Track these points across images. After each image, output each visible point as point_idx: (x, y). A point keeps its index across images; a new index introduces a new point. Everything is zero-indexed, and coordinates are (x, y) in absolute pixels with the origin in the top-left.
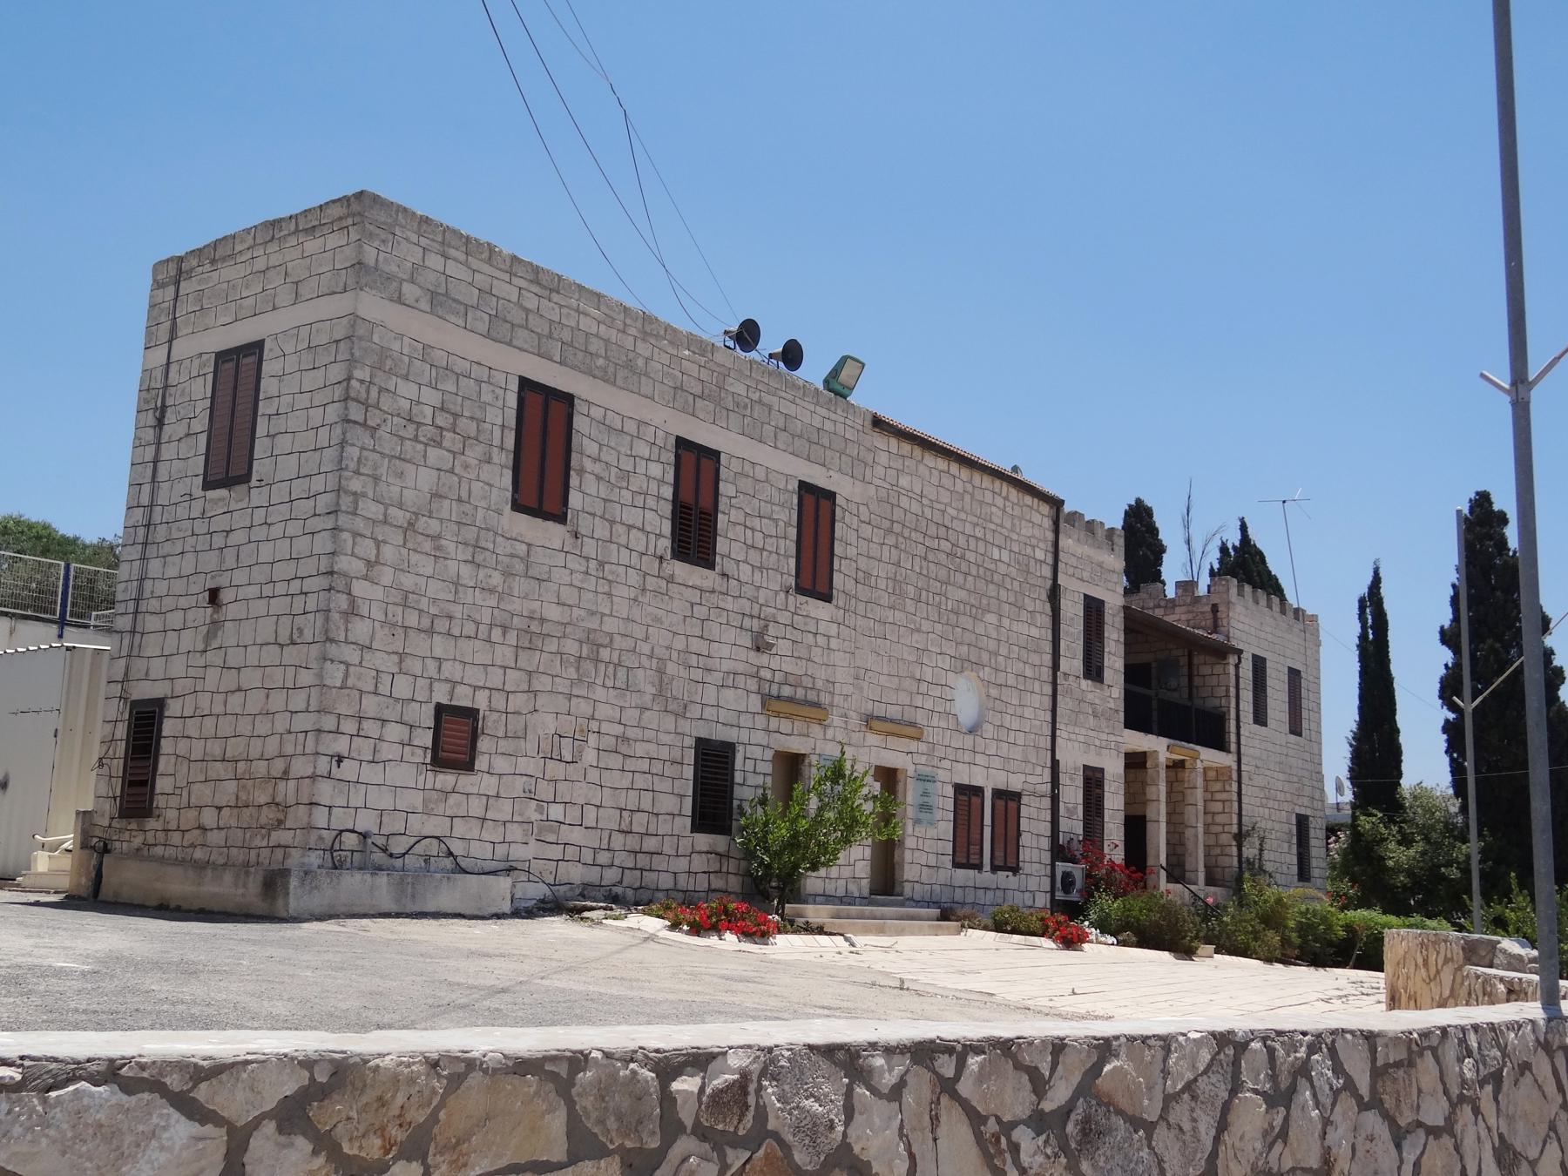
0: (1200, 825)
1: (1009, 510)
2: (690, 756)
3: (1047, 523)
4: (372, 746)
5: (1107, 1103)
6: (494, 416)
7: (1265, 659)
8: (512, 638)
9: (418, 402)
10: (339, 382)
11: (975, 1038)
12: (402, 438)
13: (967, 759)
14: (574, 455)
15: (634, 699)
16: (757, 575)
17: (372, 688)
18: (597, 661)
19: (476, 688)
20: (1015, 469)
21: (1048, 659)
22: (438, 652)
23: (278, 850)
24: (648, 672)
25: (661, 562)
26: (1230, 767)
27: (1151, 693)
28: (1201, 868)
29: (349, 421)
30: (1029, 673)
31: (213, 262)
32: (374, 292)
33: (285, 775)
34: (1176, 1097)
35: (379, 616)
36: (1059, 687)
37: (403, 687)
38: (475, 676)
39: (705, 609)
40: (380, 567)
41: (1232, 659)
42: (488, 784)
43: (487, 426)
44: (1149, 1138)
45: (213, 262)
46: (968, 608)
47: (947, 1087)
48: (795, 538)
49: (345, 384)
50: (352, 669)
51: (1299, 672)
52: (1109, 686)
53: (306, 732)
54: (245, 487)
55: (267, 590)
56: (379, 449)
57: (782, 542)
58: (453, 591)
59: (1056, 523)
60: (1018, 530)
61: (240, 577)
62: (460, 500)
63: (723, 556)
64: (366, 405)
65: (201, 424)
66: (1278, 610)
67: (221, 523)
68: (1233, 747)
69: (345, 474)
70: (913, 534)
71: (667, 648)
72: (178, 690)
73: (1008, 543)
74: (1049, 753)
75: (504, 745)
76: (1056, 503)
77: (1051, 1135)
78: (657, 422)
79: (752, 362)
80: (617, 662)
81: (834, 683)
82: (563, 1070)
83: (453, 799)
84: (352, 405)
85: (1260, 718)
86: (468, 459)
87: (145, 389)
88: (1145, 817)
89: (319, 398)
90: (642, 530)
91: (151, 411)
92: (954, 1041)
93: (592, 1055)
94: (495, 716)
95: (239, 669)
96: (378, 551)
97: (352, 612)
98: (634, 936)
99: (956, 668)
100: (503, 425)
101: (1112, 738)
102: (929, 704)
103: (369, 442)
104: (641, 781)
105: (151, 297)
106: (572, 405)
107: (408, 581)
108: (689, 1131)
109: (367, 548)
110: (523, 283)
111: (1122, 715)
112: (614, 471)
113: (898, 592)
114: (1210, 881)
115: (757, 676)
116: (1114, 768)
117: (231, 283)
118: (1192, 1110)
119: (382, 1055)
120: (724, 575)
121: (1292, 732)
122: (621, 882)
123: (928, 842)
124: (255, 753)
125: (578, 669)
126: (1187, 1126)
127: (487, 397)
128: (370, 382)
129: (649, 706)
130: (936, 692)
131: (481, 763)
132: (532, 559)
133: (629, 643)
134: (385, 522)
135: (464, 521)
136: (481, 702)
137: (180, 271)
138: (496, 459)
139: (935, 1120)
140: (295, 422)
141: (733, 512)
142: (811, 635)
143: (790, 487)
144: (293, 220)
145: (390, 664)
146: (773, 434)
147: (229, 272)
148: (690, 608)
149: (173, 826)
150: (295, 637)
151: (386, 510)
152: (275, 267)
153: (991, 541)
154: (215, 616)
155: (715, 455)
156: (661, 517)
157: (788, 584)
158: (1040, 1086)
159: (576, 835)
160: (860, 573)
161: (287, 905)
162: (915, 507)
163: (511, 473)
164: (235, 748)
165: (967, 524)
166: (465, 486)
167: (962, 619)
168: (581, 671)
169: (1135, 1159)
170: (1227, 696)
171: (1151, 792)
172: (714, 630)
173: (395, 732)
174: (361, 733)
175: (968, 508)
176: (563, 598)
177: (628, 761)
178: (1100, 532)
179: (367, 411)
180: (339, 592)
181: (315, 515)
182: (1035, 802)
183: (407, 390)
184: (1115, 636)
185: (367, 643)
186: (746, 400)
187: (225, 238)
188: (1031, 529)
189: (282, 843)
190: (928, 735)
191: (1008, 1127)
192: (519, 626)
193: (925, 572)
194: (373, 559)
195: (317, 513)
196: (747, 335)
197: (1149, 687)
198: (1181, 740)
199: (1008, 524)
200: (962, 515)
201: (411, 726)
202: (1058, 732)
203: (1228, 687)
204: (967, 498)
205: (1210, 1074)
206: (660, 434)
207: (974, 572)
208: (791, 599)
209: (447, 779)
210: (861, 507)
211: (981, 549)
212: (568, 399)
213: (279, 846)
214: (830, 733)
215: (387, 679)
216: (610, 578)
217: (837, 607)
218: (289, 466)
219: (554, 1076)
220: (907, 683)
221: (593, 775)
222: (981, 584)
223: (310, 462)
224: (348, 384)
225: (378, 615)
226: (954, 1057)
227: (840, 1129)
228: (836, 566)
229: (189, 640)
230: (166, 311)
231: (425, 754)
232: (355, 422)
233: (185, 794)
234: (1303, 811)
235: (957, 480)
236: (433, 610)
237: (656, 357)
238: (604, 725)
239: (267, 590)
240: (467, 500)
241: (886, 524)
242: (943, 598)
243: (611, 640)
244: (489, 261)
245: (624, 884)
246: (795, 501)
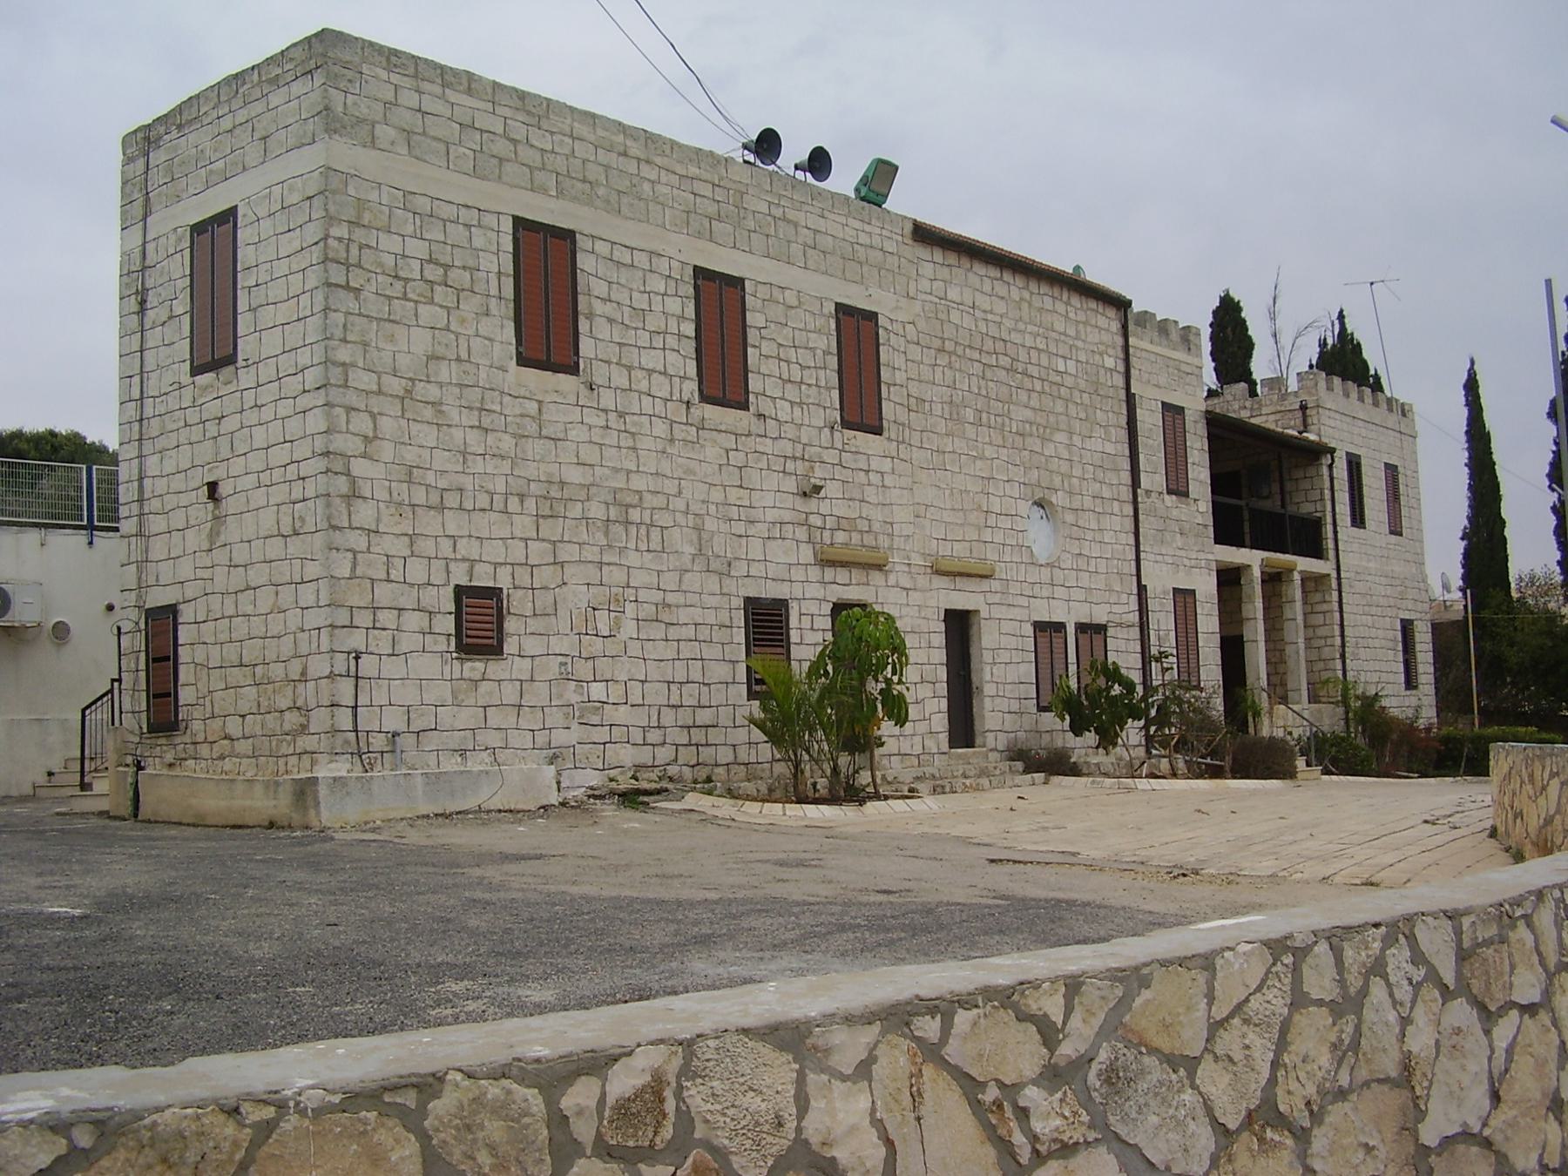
0: (1301, 640)
1: (1072, 315)
2: (739, 619)
3: (1115, 326)
4: (390, 638)
5: (1142, 1045)
6: (489, 263)
7: (1360, 456)
8: (531, 504)
9: (404, 256)
10: (316, 243)
11: (964, 992)
12: (389, 298)
13: (1045, 593)
14: (581, 298)
15: (673, 562)
16: (797, 411)
17: (384, 576)
18: (628, 523)
19: (496, 565)
20: (1077, 268)
21: (1126, 477)
22: (452, 530)
23: (305, 756)
24: (685, 529)
25: (688, 408)
26: (1329, 575)
27: (1242, 503)
28: (1304, 686)
29: (329, 285)
30: (1106, 493)
31: (180, 127)
32: (344, 139)
33: (304, 678)
34: (1222, 1023)
35: (385, 496)
36: (1140, 505)
37: (417, 571)
38: (495, 552)
39: (742, 455)
40: (378, 442)
41: (1326, 460)
42: (521, 668)
43: (483, 275)
44: (1192, 1075)
45: (180, 127)
46: (1034, 428)
47: (932, 1052)
48: (836, 367)
49: (322, 244)
50: (359, 556)
51: (1396, 467)
52: (1195, 500)
53: (319, 629)
54: (231, 368)
55: (265, 478)
56: (365, 313)
57: (821, 373)
58: (461, 460)
59: (1125, 327)
60: (1083, 337)
61: (238, 466)
62: (458, 360)
63: (757, 394)
64: (348, 266)
65: (182, 306)
66: (1371, 402)
67: (213, 409)
68: (1331, 554)
69: (332, 343)
70: (967, 350)
71: (703, 502)
72: (189, 594)
73: (1074, 351)
74: (1135, 578)
75: (534, 625)
76: (1120, 304)
77: (1069, 1092)
78: (672, 252)
79: (771, 174)
80: (649, 522)
81: (892, 524)
82: (409, 1099)
83: (484, 687)
84: (332, 267)
85: (1358, 519)
86: (462, 313)
87: (125, 274)
88: (1242, 636)
89: (298, 263)
90: (665, 373)
91: (133, 296)
92: (937, 999)
93: (449, 1077)
94: (520, 593)
95: (245, 566)
96: (375, 426)
97: (353, 495)
98: (689, 819)
99: (1025, 495)
100: (499, 272)
101: (1202, 556)
102: (999, 538)
103: (353, 306)
104: (687, 650)
105: (123, 173)
106: (574, 242)
107: (410, 455)
108: (589, 1152)
109: (362, 423)
110: (508, 112)
111: (1211, 529)
112: (627, 310)
113: (955, 417)
114: (1314, 698)
115: (806, 523)
116: (1206, 587)
117: (199, 148)
118: (1244, 1036)
119: (159, 1109)
120: (761, 416)
121: (1392, 532)
122: (676, 760)
123: (1008, 687)
124: (271, 655)
125: (606, 534)
126: (1238, 1055)
127: (478, 242)
128: (349, 239)
129: (690, 567)
130: (1005, 523)
131: (510, 647)
132: (545, 417)
133: (659, 501)
134: (380, 392)
135: (466, 382)
136: (504, 582)
137: (147, 139)
138: (494, 309)
139: (916, 1097)
140: (277, 291)
141: (764, 344)
142: (862, 474)
143: (826, 311)
144: (256, 72)
145: (400, 547)
146: (801, 253)
147: (198, 138)
148: (725, 456)
149: (200, 738)
150: (297, 526)
151: (379, 378)
152: (241, 124)
153: (1055, 351)
154: (217, 512)
155: (737, 283)
156: (685, 357)
157: (832, 419)
158: (1049, 1034)
159: (622, 714)
160: (911, 399)
161: (318, 813)
162: (968, 322)
163: (513, 324)
164: (250, 652)
165: (1027, 336)
166: (463, 342)
167: (1029, 440)
168: (610, 536)
169: (1175, 1103)
170: (1322, 499)
171: (1247, 610)
172: (753, 477)
173: (414, 621)
174: (377, 625)
175: (1026, 318)
176: (583, 457)
177: (672, 629)
178: (1174, 331)
179: (348, 271)
180: (336, 473)
181: (304, 391)
182: (1122, 633)
183: (390, 243)
184: (1198, 445)
185: (373, 527)
186: (769, 218)
187: (191, 98)
188: (1097, 335)
189: (308, 749)
190: (1001, 571)
191: (1011, 1089)
192: (539, 493)
193: (984, 393)
194: (371, 434)
195: (306, 388)
196: (767, 144)
197: (1240, 499)
198: (1275, 551)
199: (1072, 332)
200: (1021, 326)
201: (430, 613)
202: (1143, 555)
203: (1322, 490)
204: (1025, 306)
205: (1265, 990)
206: (675, 264)
207: (1038, 388)
208: (837, 435)
209: (475, 667)
210: (907, 326)
211: (1045, 362)
212: (567, 237)
213: (306, 752)
214: (892, 579)
215: (399, 563)
216: (633, 430)
217: (889, 439)
218: (272, 342)
219: (402, 1112)
220: (973, 517)
221: (634, 649)
222: (1047, 401)
223: (294, 335)
224: (325, 244)
225: (382, 495)
226: (938, 1017)
227: (791, 1125)
228: (884, 394)
229: (195, 539)
230: (138, 188)
231: (448, 640)
232: (337, 286)
233: (208, 704)
234: (1407, 616)
235: (1012, 287)
236: (442, 484)
237: (664, 179)
238: (641, 592)
239: (265, 478)
240: (466, 358)
241: (937, 343)
242: (1007, 420)
243: (641, 499)
244: (469, 91)
245: (680, 762)
246: (833, 326)
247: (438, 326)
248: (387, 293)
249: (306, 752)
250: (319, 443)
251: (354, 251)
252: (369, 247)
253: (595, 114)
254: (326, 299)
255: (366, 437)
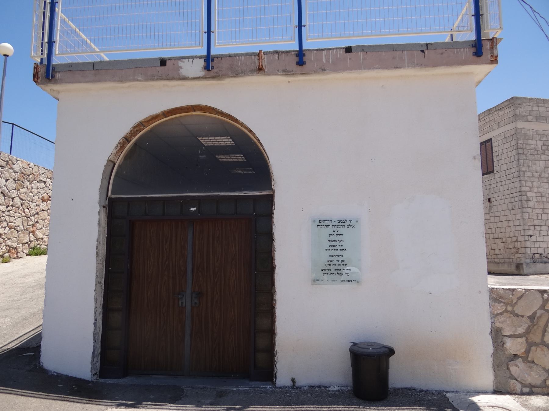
9: (537, 145)
12: (534, 155)
17: (536, 218)
33: (517, 241)
61: (496, 195)
64: (523, 149)
103: (525, 158)
107: (541, 190)
109: (529, 184)
128: (523, 143)
144: (495, 108)
145: (540, 211)
164: (501, 235)
174: (535, 229)
183: (533, 142)
185: (533, 207)
213: (518, 258)
218: (504, 167)
233: (490, 246)
247: (547, 160)
248: (533, 154)
249: (518, 258)
250: (518, 190)
251: (524, 145)
252: (528, 144)
253: (363, 46)
254: (518, 157)
255: (530, 187)
